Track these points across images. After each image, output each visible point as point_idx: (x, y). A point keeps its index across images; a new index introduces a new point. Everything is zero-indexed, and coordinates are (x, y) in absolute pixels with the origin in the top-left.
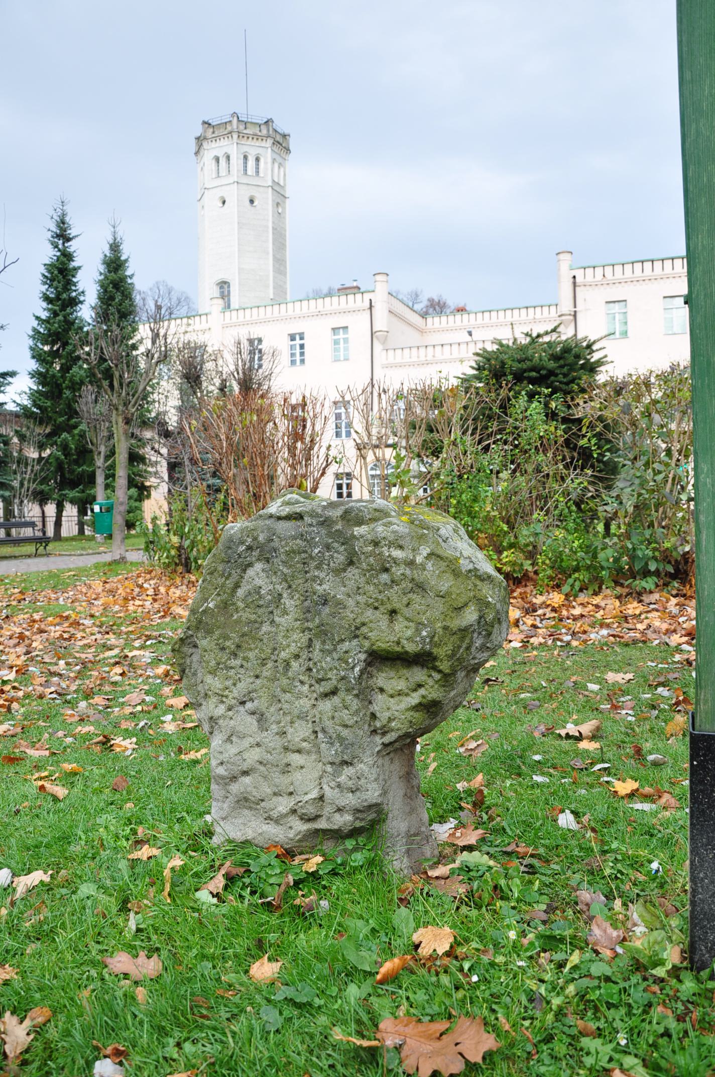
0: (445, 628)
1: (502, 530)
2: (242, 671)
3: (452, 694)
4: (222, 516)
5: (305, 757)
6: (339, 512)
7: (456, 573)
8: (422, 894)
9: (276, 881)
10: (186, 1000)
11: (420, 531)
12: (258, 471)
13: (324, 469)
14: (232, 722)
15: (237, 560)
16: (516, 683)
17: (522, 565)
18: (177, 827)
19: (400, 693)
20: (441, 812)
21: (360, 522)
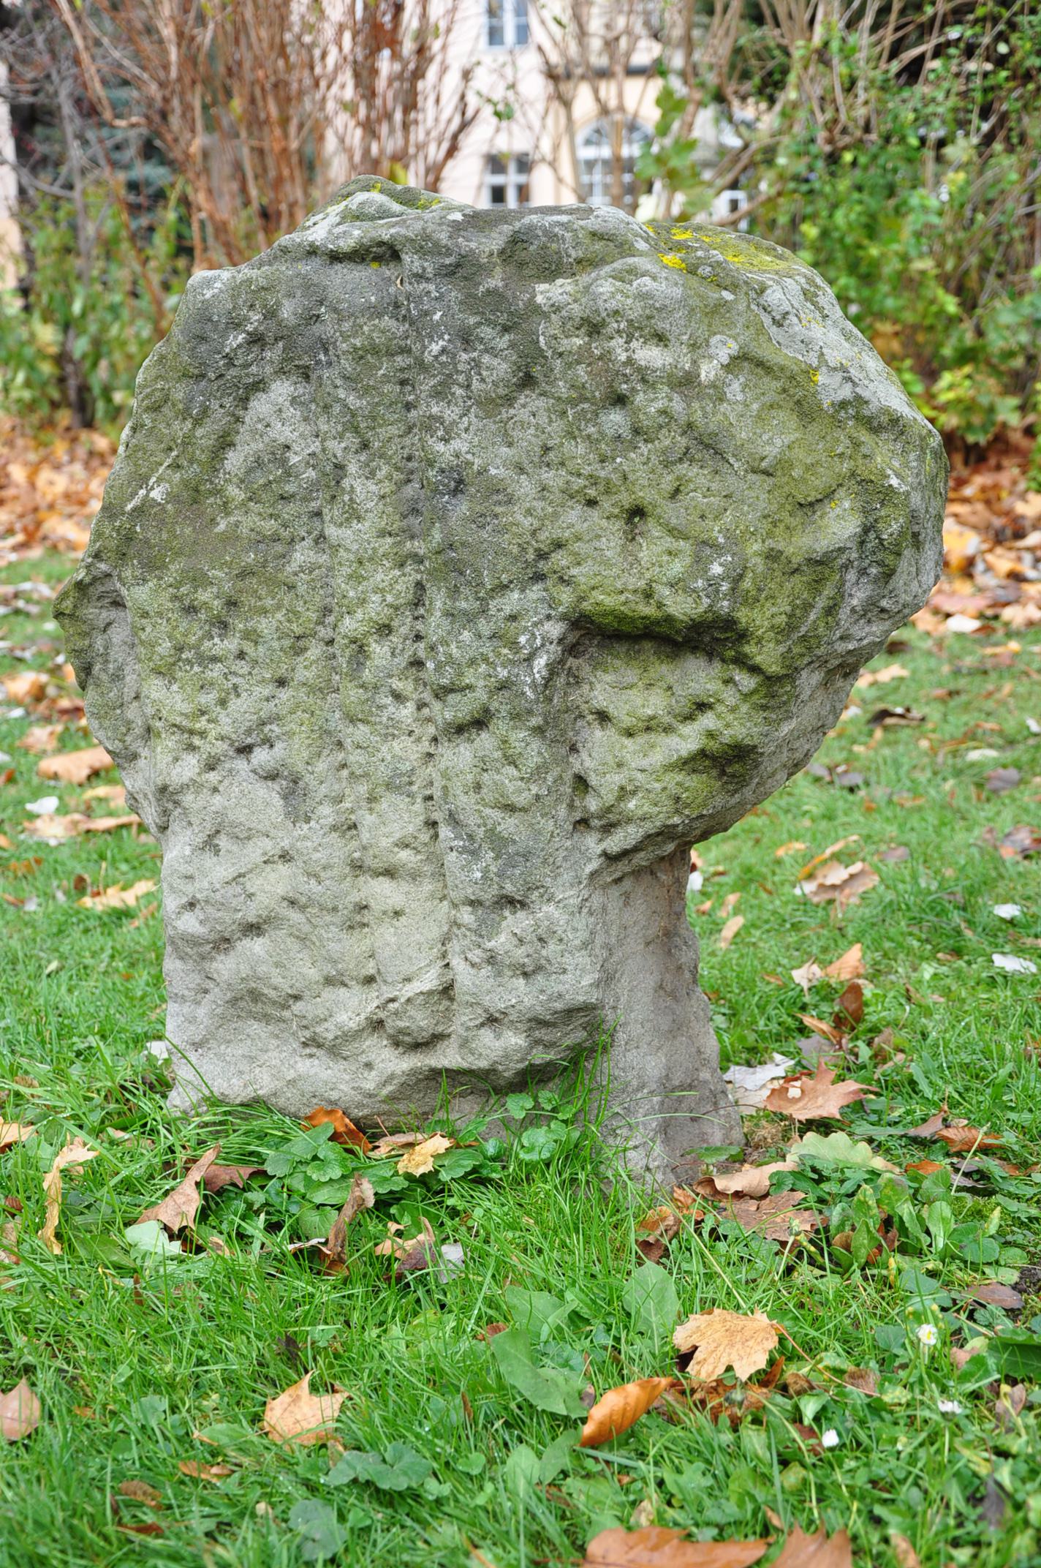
0: (772, 556)
1: (941, 312)
2: (242, 667)
3: (786, 728)
4: (175, 272)
5: (405, 886)
6: (494, 241)
7: (806, 410)
8: (698, 1231)
9: (331, 1195)
10: (101, 1489)
11: (714, 295)
12: (272, 140)
13: (455, 137)
14: (217, 799)
15: (222, 370)
16: (959, 722)
17: (991, 410)
18: (76, 1071)
19: (650, 726)
20: (751, 1038)
21: (551, 270)
